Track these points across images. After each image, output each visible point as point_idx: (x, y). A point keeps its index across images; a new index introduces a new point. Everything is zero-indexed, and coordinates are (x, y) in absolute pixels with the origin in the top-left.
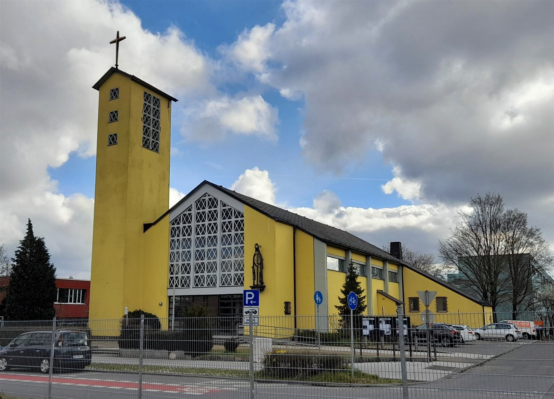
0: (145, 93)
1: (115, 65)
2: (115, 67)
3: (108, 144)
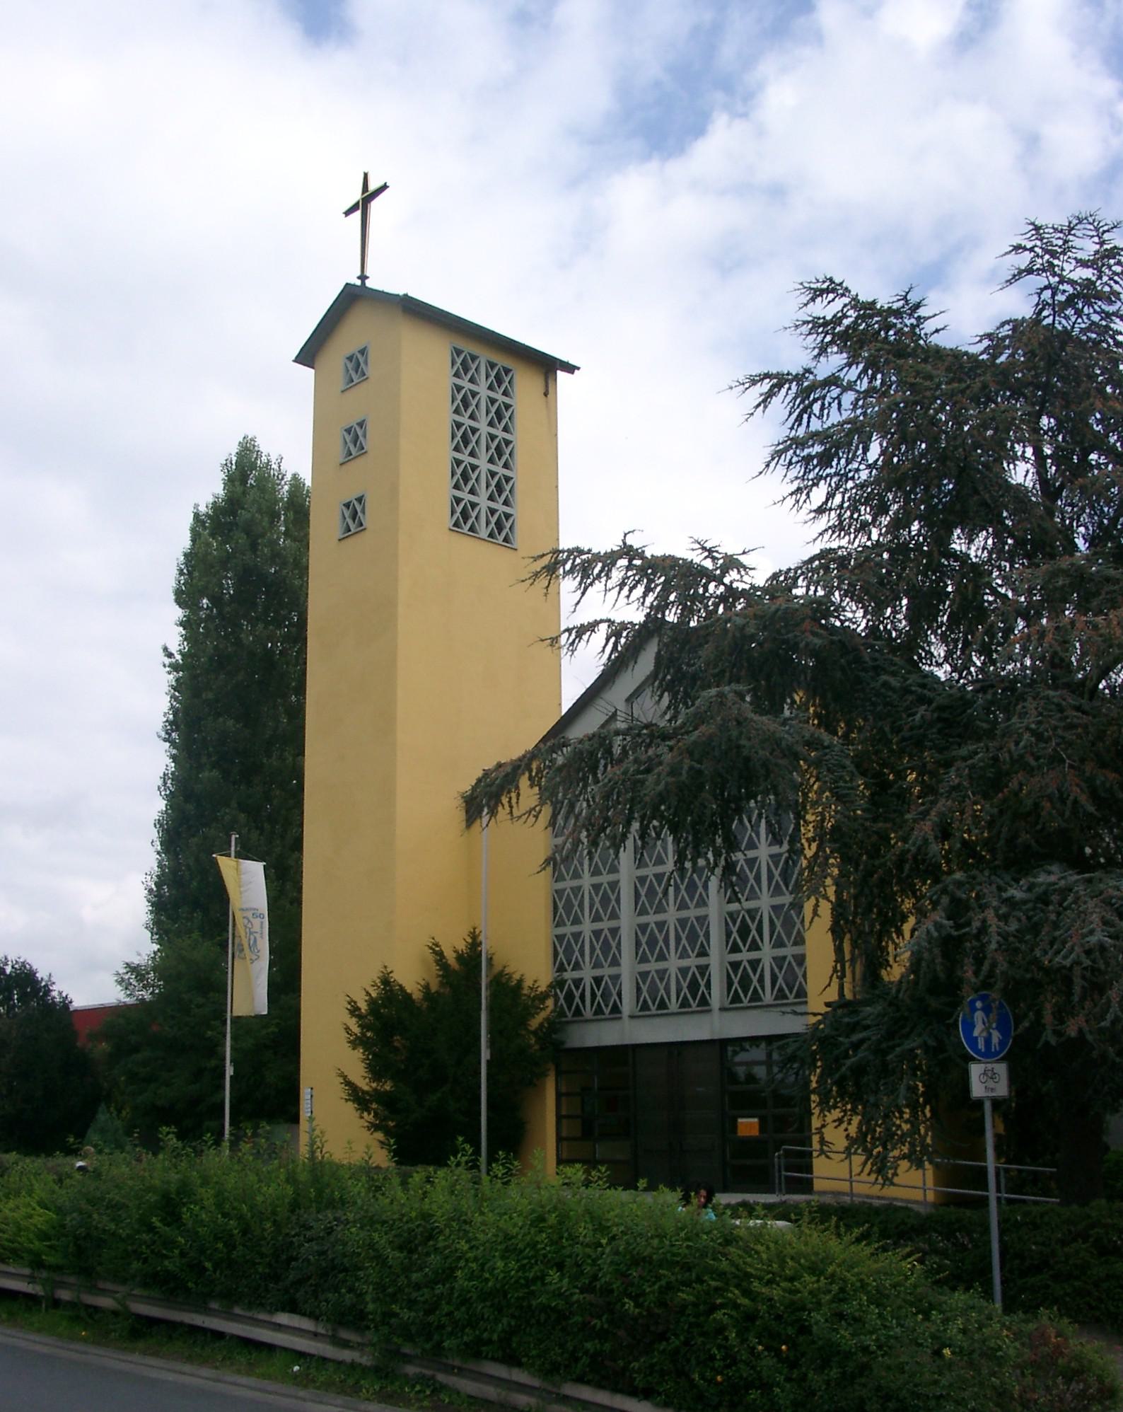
0: (459, 352)
1: (359, 278)
2: (358, 283)
3: (339, 533)
